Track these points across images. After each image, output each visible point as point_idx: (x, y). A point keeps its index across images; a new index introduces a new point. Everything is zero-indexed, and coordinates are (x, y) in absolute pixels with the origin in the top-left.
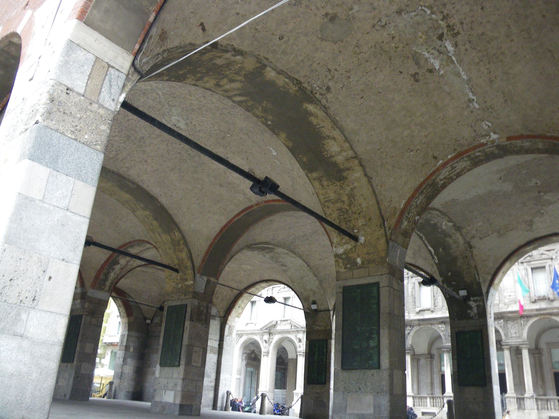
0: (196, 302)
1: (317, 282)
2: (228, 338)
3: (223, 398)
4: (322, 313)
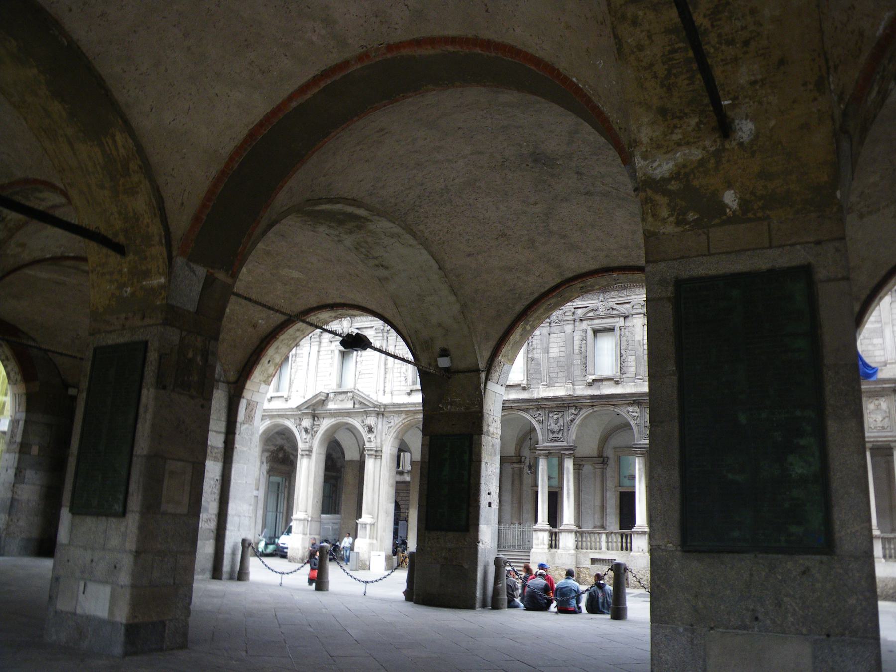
0: (174, 336)
1: (457, 307)
2: (244, 427)
3: (234, 553)
4: (461, 375)
